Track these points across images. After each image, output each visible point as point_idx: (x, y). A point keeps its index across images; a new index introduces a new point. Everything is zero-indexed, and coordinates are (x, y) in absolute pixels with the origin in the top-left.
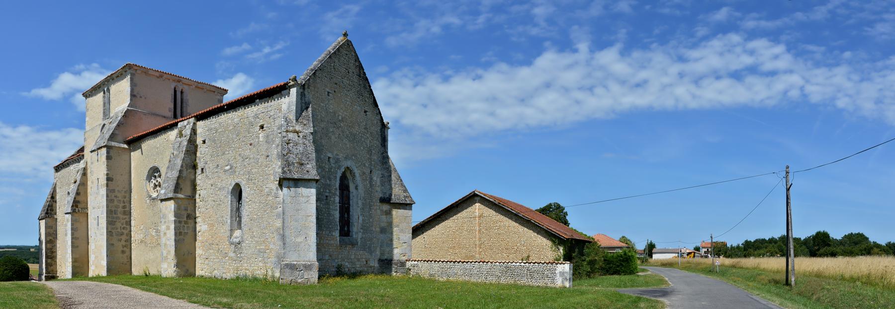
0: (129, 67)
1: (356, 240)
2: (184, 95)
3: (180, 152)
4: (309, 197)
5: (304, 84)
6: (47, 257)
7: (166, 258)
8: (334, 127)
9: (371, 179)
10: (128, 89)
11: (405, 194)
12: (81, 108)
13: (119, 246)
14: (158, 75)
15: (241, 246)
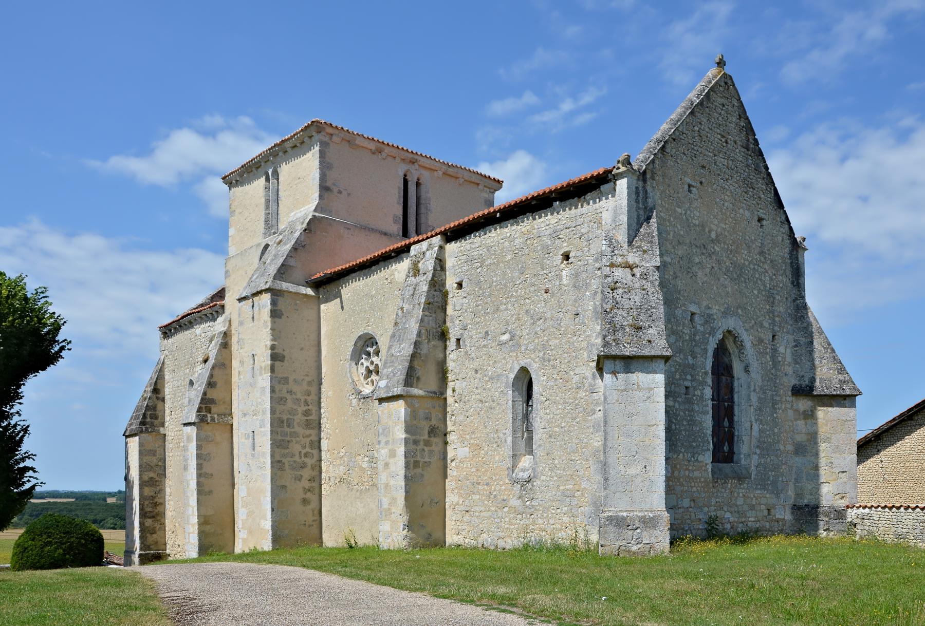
0: (316, 127)
1: (747, 469)
2: (423, 189)
3: (414, 306)
4: (650, 389)
5: (645, 172)
6: (143, 515)
7: (389, 512)
8: (703, 254)
9: (775, 350)
10: (316, 175)
11: (841, 377)
12: (218, 209)
13: (297, 490)
14: (373, 148)
15: (533, 486)
